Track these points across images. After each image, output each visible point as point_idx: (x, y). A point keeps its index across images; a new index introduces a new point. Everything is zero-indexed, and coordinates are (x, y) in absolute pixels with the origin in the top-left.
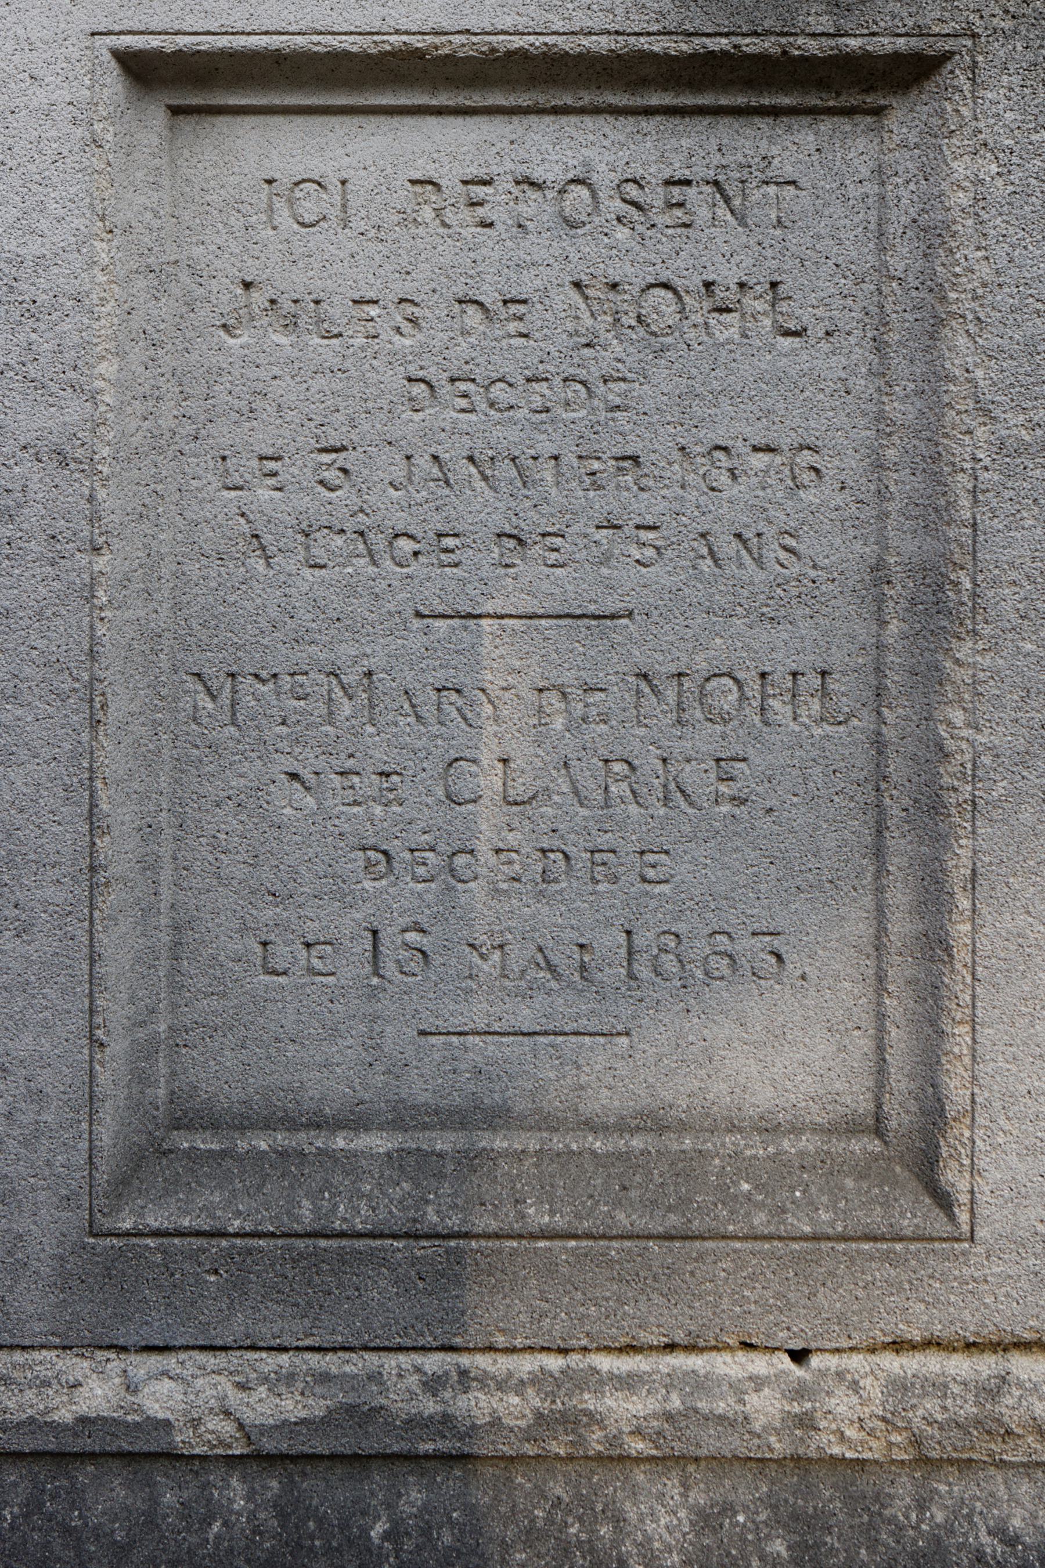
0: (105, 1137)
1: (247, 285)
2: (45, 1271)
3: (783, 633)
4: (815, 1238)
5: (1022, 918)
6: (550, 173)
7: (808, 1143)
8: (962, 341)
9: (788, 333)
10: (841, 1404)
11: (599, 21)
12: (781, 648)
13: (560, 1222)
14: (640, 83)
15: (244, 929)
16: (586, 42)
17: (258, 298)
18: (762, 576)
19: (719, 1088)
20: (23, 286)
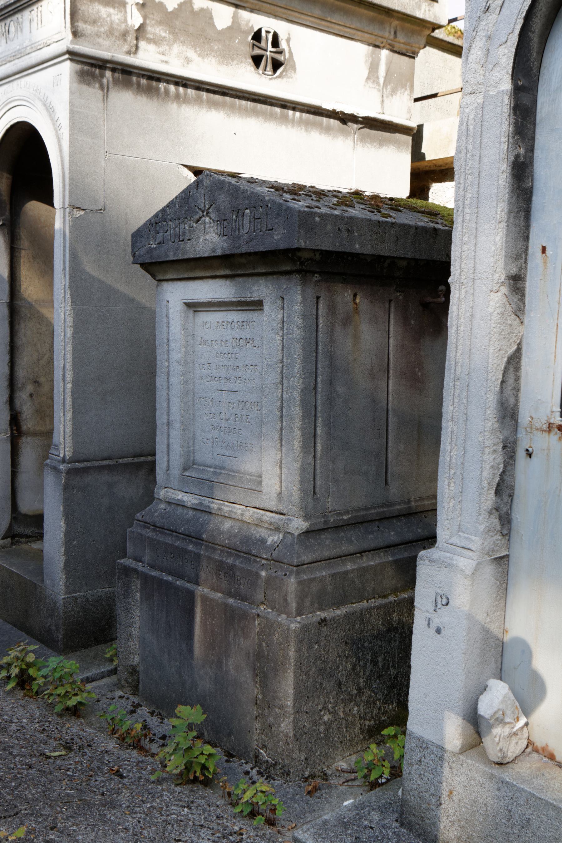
4: (247, 489)
10: (247, 513)
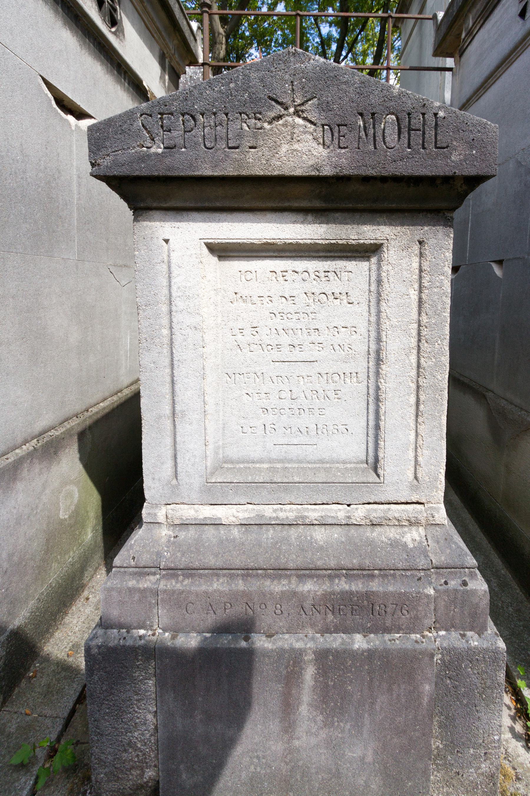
0: (209, 464)
1: (236, 293)
3: (348, 364)
5: (395, 421)
7: (352, 465)
8: (384, 304)
9: (349, 303)
11: (308, 237)
13: (301, 480)
14: (318, 251)
16: (305, 241)
17: (238, 296)
19: (334, 455)
20: (186, 292)
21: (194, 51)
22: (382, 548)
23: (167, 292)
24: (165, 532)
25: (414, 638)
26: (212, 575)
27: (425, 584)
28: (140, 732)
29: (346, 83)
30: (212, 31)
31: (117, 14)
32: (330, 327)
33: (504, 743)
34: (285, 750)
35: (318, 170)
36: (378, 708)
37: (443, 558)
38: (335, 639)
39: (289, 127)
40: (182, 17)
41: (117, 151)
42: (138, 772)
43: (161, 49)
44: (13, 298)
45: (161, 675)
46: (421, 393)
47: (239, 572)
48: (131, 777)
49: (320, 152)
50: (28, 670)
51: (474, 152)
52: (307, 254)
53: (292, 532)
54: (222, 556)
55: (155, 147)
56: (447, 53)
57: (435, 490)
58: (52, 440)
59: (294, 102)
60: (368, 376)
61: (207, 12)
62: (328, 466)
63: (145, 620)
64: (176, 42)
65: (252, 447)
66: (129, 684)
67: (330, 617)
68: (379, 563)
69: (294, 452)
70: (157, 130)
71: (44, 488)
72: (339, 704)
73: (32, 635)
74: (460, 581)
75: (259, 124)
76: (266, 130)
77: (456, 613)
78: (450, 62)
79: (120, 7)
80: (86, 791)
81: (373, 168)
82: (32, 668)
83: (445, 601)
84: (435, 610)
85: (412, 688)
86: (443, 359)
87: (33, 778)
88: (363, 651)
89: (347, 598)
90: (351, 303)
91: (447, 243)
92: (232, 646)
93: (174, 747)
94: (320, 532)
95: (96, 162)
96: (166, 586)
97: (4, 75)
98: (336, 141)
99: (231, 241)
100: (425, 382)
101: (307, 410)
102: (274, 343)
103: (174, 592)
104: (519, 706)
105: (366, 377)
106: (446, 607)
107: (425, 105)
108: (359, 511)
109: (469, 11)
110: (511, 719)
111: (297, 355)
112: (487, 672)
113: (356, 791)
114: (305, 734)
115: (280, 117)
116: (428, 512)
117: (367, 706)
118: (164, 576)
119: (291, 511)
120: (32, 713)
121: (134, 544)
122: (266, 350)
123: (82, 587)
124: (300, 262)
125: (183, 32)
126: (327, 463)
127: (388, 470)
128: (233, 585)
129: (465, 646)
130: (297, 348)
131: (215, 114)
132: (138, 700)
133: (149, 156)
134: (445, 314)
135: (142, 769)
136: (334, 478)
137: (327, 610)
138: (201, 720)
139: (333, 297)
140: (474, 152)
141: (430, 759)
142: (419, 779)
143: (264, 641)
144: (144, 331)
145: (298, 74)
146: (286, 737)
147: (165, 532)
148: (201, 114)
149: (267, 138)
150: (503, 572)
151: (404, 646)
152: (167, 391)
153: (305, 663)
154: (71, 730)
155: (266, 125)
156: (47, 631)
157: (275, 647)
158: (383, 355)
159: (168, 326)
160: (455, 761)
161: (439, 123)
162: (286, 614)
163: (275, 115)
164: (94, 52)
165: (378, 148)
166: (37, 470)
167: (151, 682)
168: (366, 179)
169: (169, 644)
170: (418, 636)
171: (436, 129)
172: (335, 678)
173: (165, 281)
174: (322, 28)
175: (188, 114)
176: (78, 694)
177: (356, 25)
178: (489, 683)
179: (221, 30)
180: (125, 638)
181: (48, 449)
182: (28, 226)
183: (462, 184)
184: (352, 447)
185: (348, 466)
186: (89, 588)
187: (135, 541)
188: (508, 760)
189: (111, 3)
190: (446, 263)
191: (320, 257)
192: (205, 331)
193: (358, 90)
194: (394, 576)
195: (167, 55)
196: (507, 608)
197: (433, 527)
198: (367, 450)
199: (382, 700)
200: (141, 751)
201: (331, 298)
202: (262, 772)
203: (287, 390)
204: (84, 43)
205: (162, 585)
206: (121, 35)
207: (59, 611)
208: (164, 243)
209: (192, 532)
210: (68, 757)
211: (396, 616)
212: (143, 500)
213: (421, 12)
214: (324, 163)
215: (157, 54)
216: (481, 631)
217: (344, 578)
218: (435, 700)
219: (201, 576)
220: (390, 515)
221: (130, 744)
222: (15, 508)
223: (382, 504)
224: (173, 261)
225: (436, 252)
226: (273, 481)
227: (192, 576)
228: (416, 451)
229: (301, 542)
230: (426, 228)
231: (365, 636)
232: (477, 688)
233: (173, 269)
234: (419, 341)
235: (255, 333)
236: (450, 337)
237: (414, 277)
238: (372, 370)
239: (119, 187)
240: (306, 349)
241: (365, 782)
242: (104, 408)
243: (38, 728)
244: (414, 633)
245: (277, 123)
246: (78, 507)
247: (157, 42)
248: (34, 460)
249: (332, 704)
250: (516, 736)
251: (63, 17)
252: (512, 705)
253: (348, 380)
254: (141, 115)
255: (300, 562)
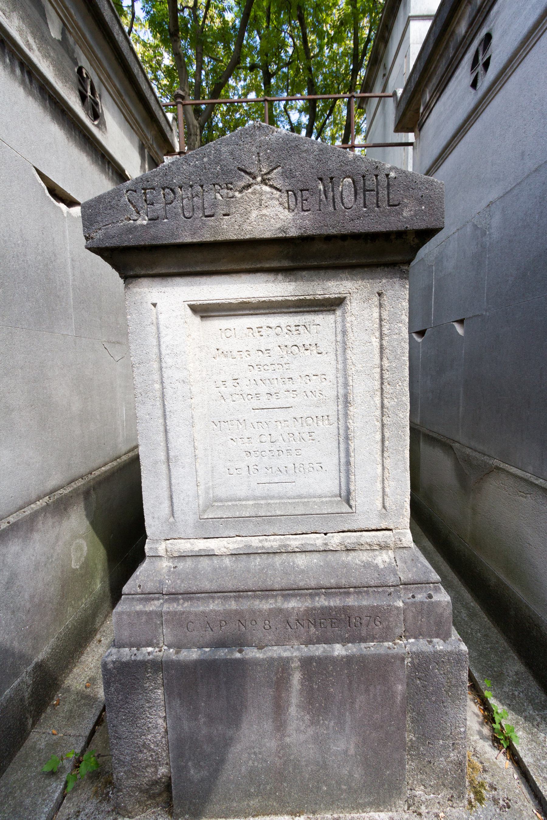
0: (201, 502)
1: (218, 350)
2: (192, 526)
3: (320, 409)
5: (363, 457)
6: (273, 325)
7: (328, 499)
8: (349, 352)
9: (319, 353)
11: (279, 294)
12: (320, 412)
13: (282, 514)
14: (289, 307)
15: (225, 467)
16: (277, 298)
17: (220, 352)
18: (316, 399)
19: (311, 491)
20: (174, 350)
21: (171, 141)
22: (356, 569)
23: (157, 351)
24: (165, 564)
25: (387, 645)
26: (209, 598)
27: (395, 598)
28: (153, 735)
29: (306, 151)
30: (187, 123)
31: (99, 108)
32: (302, 376)
33: (473, 743)
34: (278, 746)
35: (285, 232)
36: (357, 706)
37: (410, 576)
38: (317, 649)
39: (258, 195)
40: (158, 108)
41: (107, 225)
42: (153, 770)
43: (140, 140)
44: (21, 368)
45: (168, 684)
46: (386, 430)
47: (232, 594)
48: (147, 774)
49: (286, 216)
50: (52, 699)
51: (423, 207)
52: (279, 311)
53: (276, 559)
54: (216, 581)
55: (140, 219)
56: (407, 128)
57: (401, 517)
58: (62, 498)
59: (261, 171)
60: (338, 419)
61: (181, 103)
62: (306, 500)
63: (152, 639)
64: (153, 132)
65: (239, 486)
66: (141, 694)
67: (313, 629)
68: (354, 581)
69: (276, 489)
70: (141, 204)
71: (58, 540)
72: (323, 705)
73: (54, 669)
74: (425, 595)
75: (231, 194)
76: (238, 199)
77: (425, 622)
78: (411, 137)
79: (100, 101)
80: (109, 792)
81: (333, 228)
82: (55, 698)
83: (413, 612)
84: (404, 620)
85: (386, 689)
86: (404, 398)
87: (63, 783)
88: (343, 657)
89: (326, 612)
90: (320, 353)
91: (403, 294)
92: (229, 657)
93: (182, 747)
94: (301, 558)
95: (89, 236)
96: (169, 608)
97: (3, 167)
98: (300, 205)
99: (211, 302)
100: (389, 420)
101: (285, 451)
102: (253, 392)
103: (176, 613)
104: (486, 713)
105: (336, 419)
106: (414, 617)
107: (377, 167)
108: (335, 538)
109: (426, 86)
110: (480, 724)
111: (274, 402)
112: (452, 673)
113: (341, 780)
114: (295, 732)
115: (249, 186)
116: (396, 537)
117: (348, 706)
118: (166, 601)
119: (274, 540)
120: (58, 733)
121: (140, 575)
122: (246, 400)
123: (95, 631)
124: (273, 318)
125: (159, 123)
126: (305, 498)
127: (359, 501)
128: (227, 606)
129: (432, 650)
130: (274, 396)
131: (191, 186)
132: (150, 707)
133: (136, 228)
134: (404, 358)
135: (156, 767)
136: (311, 511)
137: (310, 624)
138: (205, 723)
139: (304, 349)
140: (423, 207)
141: (405, 750)
142: (396, 768)
143: (256, 653)
144: (139, 386)
145: (264, 146)
146: (278, 735)
147: (165, 564)
148: (179, 187)
149: (238, 205)
150: (472, 604)
151: (378, 652)
152: (162, 439)
153: (292, 670)
154: (92, 746)
155: (237, 194)
156: (66, 667)
157: (265, 657)
158: (350, 398)
159: (159, 381)
160: (427, 751)
161: (390, 183)
162: (273, 628)
163: (244, 184)
164: (80, 143)
165: (337, 208)
166: (50, 524)
167: (160, 691)
168: (328, 238)
169: (174, 657)
170: (391, 643)
171: (388, 189)
172: (319, 682)
173: (155, 341)
174: (291, 115)
175: (168, 188)
176: (96, 717)
177: (323, 110)
178: (454, 682)
179: (196, 123)
180: (135, 655)
181: (59, 506)
182: (31, 304)
183: (414, 238)
184: (327, 483)
185: (324, 499)
186: (100, 632)
187: (140, 572)
188: (476, 756)
189: (93, 98)
190: (403, 311)
191: (291, 313)
192: (192, 384)
193: (317, 157)
194: (367, 593)
195: (146, 145)
196: (476, 634)
197: (401, 550)
198: (340, 484)
199: (361, 699)
200: (154, 752)
201: (302, 349)
202: (259, 766)
203: (267, 434)
204: (71, 135)
205: (166, 608)
206: (103, 127)
207: (76, 650)
208: (153, 307)
209: (189, 563)
210: (92, 765)
211: (370, 627)
212: (146, 537)
213: (384, 91)
214: (290, 225)
215: (137, 145)
216: (446, 637)
217: (323, 596)
218: (408, 698)
219: (198, 599)
220: (362, 541)
221: (144, 745)
222: (33, 555)
223: (355, 531)
224: (162, 322)
225: (393, 302)
226: (258, 515)
227: (191, 599)
228: (383, 483)
229: (284, 568)
230: (384, 281)
231: (343, 646)
232: (444, 687)
233: (161, 330)
234: (382, 383)
235: (236, 384)
236: (409, 379)
237: (375, 326)
238: (341, 413)
239: (111, 258)
240: (282, 397)
241: (349, 772)
242: (106, 472)
243: (64, 745)
244: (387, 641)
245: (247, 192)
246: (87, 559)
247: (136, 133)
248: (48, 514)
249: (318, 705)
250: (483, 737)
251: (51, 112)
252: (480, 713)
253: (320, 423)
254: (127, 191)
255: (284, 583)
